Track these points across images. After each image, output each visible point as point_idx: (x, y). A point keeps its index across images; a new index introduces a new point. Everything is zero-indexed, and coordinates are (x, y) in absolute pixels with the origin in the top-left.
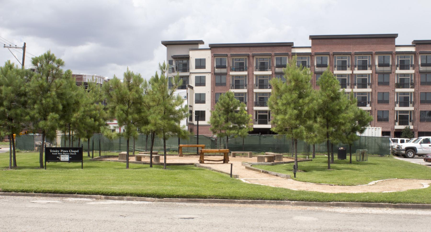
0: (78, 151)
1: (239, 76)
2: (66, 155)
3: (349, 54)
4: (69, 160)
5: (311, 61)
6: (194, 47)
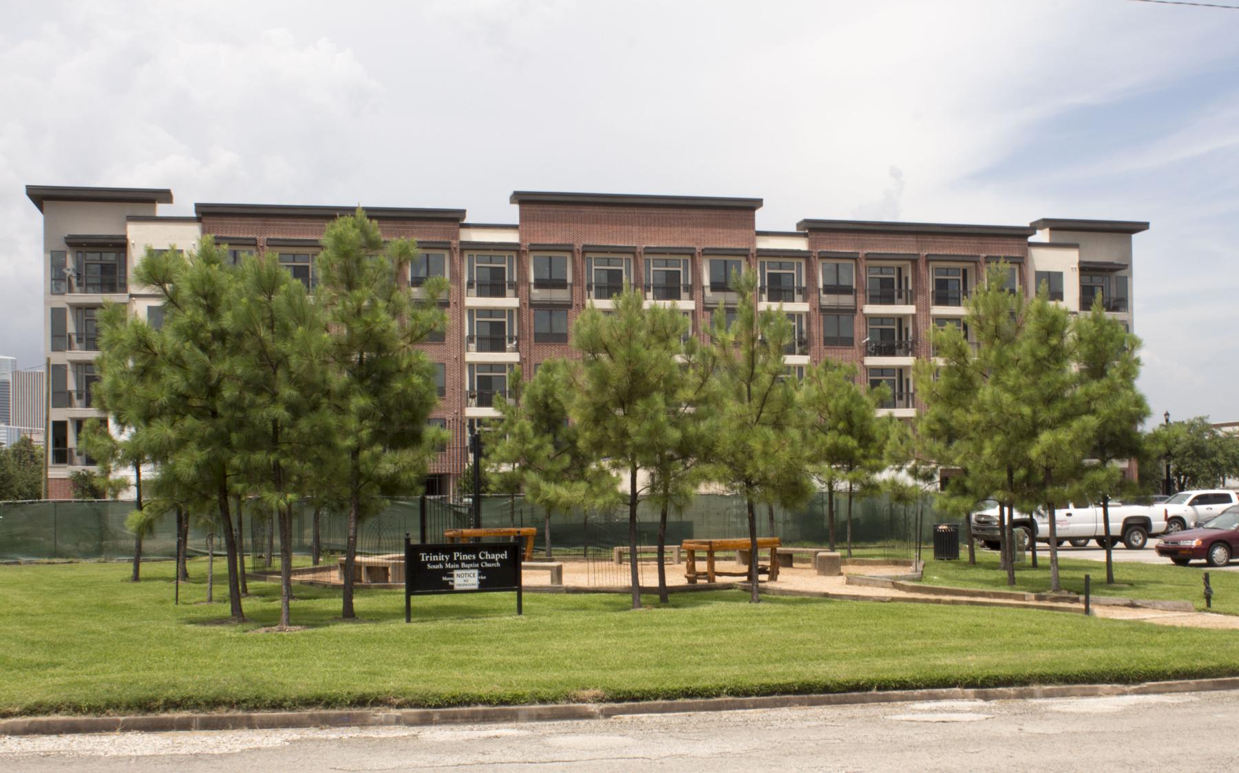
0: (505, 556)
1: (882, 319)
2: (471, 568)
3: (631, 250)
4: (480, 586)
5: (518, 269)
6: (140, 209)
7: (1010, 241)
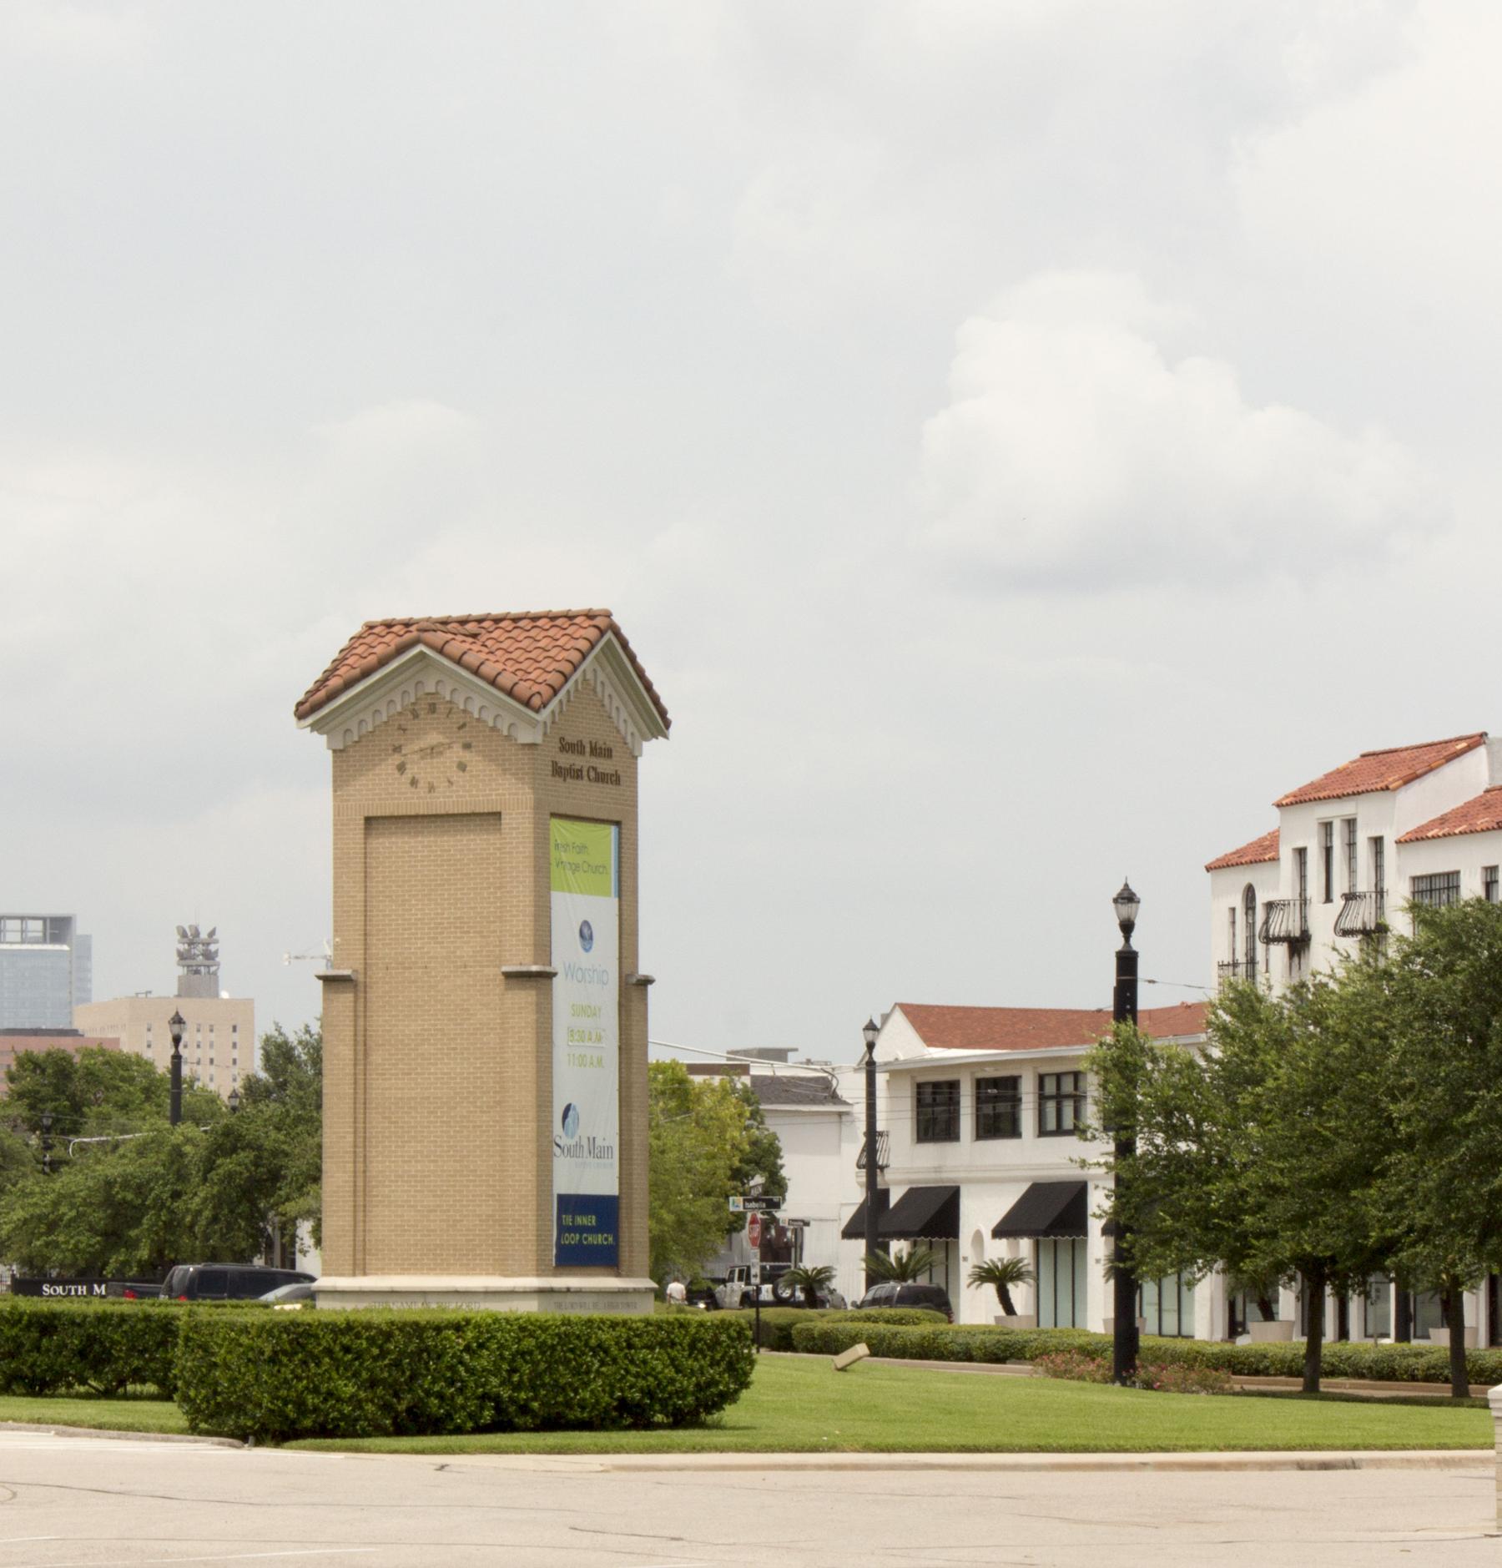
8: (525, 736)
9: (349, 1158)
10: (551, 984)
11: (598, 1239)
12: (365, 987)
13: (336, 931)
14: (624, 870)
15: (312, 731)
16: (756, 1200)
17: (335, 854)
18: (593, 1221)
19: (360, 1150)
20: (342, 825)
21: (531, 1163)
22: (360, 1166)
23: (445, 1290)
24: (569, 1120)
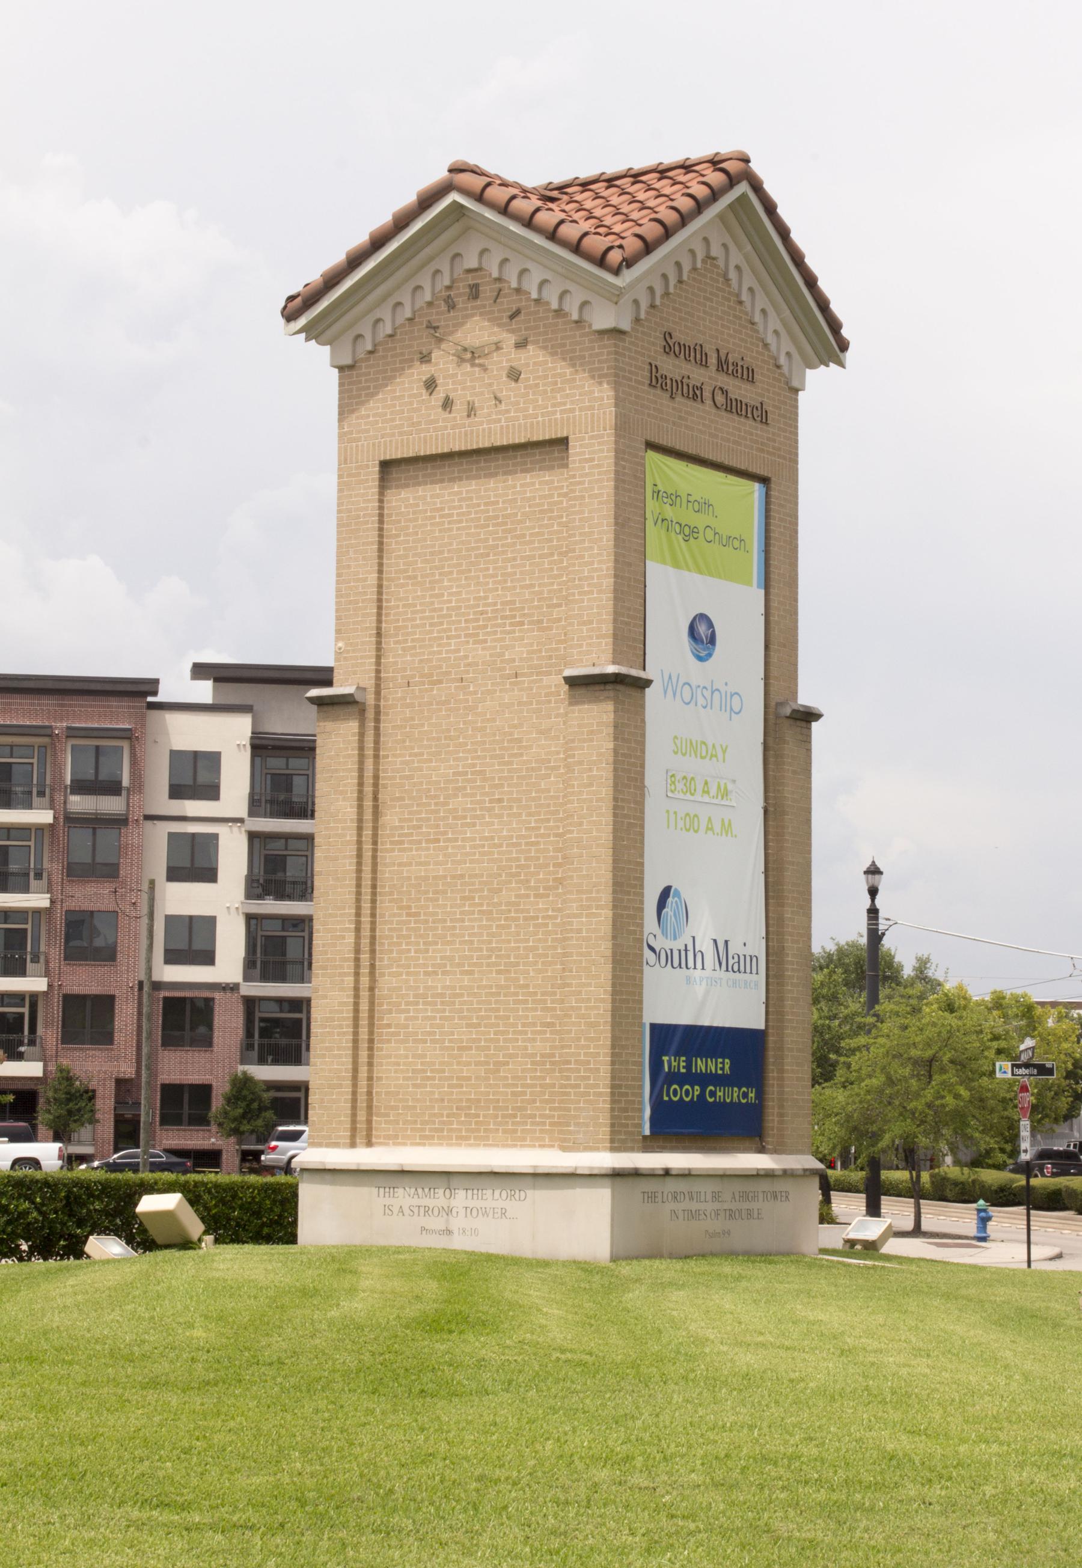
7: (114, 702)
8: (603, 318)
9: (349, 967)
10: (643, 697)
11: (733, 1095)
12: (378, 713)
13: (338, 631)
14: (774, 549)
15: (307, 339)
16: (1027, 1065)
17: (339, 519)
18: (727, 1067)
19: (365, 957)
20: (349, 475)
21: (604, 972)
22: (365, 981)
23: (546, 1171)
24: (667, 911)
